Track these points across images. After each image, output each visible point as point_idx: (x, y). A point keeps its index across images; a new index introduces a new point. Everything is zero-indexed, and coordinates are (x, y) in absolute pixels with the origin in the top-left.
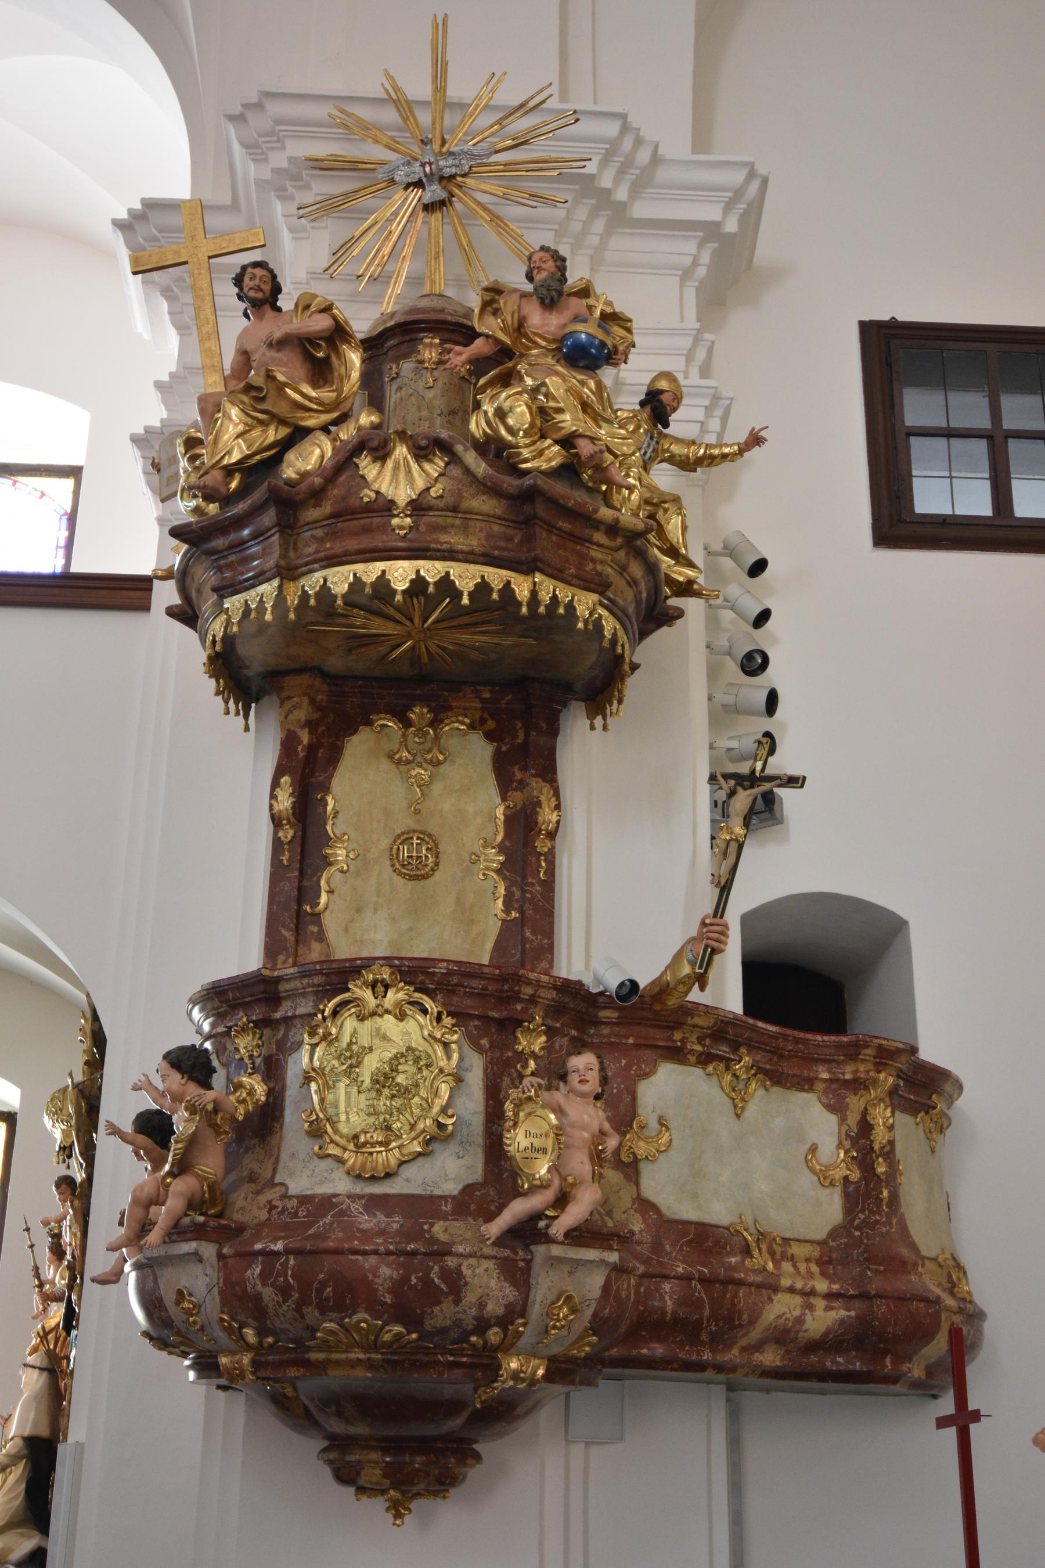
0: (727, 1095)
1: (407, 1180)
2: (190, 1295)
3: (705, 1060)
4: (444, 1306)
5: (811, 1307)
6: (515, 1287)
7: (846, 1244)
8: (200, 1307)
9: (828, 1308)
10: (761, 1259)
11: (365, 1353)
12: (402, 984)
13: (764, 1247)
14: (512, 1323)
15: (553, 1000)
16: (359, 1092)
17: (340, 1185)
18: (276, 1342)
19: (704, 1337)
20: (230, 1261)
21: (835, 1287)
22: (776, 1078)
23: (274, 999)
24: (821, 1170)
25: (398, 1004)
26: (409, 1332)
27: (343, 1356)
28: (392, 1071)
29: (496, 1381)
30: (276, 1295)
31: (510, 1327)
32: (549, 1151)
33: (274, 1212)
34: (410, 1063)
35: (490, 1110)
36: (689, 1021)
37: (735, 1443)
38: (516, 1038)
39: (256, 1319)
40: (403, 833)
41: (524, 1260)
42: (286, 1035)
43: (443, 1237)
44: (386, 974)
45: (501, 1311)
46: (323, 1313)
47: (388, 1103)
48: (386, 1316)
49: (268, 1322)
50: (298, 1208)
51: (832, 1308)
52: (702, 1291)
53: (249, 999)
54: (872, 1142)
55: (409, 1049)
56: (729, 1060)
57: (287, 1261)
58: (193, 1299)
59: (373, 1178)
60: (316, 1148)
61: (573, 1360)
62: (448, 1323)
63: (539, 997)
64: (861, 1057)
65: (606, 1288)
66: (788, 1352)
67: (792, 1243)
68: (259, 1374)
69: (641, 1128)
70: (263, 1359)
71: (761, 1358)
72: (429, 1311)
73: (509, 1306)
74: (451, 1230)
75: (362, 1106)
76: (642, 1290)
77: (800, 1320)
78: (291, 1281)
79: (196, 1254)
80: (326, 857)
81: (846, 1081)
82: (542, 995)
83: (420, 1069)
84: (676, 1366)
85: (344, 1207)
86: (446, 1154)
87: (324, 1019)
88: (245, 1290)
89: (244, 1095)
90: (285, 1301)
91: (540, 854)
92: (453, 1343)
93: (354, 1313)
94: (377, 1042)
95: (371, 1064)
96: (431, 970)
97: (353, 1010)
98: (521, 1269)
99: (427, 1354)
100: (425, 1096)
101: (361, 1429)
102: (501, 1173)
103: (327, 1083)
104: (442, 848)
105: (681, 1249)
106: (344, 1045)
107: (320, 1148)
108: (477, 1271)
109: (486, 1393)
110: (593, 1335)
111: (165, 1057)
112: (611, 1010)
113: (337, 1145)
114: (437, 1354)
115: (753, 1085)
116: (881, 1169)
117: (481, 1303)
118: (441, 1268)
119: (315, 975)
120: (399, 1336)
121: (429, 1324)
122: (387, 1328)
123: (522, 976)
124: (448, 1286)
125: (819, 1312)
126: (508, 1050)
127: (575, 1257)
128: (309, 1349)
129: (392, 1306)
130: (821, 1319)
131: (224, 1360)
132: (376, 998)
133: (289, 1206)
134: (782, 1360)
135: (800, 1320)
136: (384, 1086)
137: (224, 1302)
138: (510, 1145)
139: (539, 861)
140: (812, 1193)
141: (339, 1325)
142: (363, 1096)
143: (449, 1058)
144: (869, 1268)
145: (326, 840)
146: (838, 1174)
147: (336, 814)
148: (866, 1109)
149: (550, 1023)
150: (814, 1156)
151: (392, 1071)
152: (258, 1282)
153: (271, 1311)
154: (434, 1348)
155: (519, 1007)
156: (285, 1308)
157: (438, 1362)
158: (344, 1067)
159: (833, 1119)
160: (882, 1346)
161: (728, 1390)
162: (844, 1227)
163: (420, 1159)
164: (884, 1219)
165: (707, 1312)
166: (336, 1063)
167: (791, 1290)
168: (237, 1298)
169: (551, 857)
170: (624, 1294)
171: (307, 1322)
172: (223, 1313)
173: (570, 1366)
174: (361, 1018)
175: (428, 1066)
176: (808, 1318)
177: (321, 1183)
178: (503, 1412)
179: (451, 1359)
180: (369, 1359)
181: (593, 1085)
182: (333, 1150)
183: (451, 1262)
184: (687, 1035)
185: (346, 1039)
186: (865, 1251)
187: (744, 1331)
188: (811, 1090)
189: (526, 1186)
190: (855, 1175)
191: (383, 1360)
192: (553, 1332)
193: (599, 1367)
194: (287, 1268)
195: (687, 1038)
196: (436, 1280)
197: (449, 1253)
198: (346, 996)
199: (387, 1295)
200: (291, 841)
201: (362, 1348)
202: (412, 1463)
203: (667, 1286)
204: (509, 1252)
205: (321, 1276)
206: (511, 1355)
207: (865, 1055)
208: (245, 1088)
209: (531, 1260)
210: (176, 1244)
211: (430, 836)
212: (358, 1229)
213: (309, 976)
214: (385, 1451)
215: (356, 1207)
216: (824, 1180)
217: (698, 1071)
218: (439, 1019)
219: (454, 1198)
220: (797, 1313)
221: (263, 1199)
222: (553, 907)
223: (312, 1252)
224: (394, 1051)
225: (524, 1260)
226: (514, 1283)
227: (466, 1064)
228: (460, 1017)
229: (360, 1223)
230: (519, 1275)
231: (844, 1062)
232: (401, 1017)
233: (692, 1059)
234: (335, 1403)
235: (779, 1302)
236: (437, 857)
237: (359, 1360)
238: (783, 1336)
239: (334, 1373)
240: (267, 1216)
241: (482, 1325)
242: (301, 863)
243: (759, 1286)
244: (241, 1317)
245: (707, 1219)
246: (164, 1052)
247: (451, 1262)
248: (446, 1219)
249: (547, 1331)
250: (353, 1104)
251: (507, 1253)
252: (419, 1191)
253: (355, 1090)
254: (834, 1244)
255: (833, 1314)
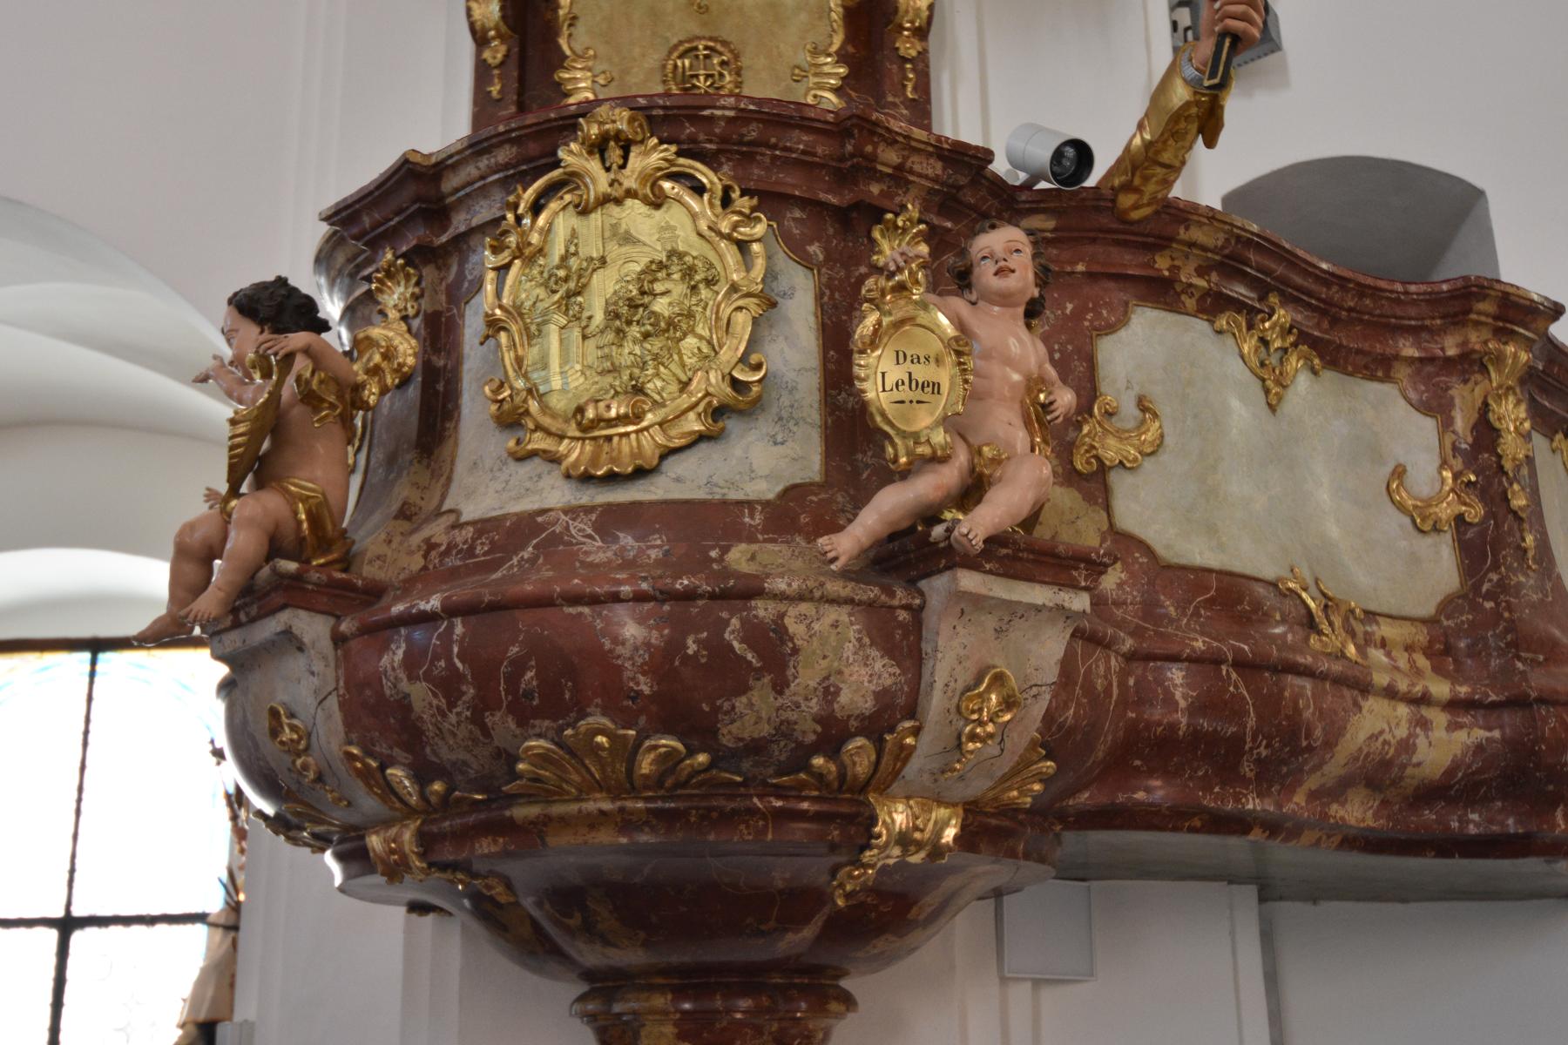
0: (1251, 370)
1: (678, 480)
2: (292, 715)
3: (1212, 305)
4: (755, 696)
5: (1424, 724)
6: (892, 658)
7: (1472, 623)
8: (309, 735)
9: (1453, 727)
10: (1332, 638)
11: (613, 800)
12: (655, 141)
13: (1337, 621)
14: (892, 730)
15: (935, 180)
16: (584, 337)
17: (554, 494)
18: (450, 790)
19: (1247, 769)
20: (354, 644)
21: (1463, 690)
22: (1331, 356)
23: (438, 213)
24: (1416, 507)
25: (652, 179)
26: (691, 752)
27: (573, 808)
28: (643, 293)
29: (869, 847)
30: (435, 695)
31: (888, 737)
32: (945, 389)
33: (433, 553)
34: (676, 276)
35: (832, 367)
36: (1183, 234)
37: (1272, 980)
38: (873, 241)
39: (406, 747)
40: (681, 43)
41: (907, 607)
42: (461, 274)
43: (746, 568)
44: (621, 120)
45: (867, 705)
46: (522, 723)
47: (637, 351)
48: (642, 720)
49: (428, 750)
50: (474, 540)
51: (1460, 726)
52: (1241, 684)
53: (397, 219)
54: (1500, 457)
55: (672, 253)
56: (1251, 312)
57: (451, 628)
58: (295, 722)
59: (612, 478)
60: (512, 443)
61: (1010, 811)
62: (765, 730)
63: (911, 172)
64: (1473, 316)
65: (1067, 666)
66: (1385, 803)
67: (1380, 619)
68: (435, 858)
69: (1110, 414)
70: (435, 829)
71: (1341, 813)
72: (726, 706)
73: (882, 696)
74: (763, 557)
75: (590, 360)
76: (1131, 682)
77: (1407, 746)
78: (459, 665)
79: (288, 633)
80: (559, 84)
81: (1448, 360)
82: (917, 168)
83: (694, 288)
84: (1197, 823)
85: (558, 529)
86: (752, 436)
87: (519, 219)
88: (380, 694)
89: (377, 358)
90: (451, 705)
91: (905, 60)
92: (779, 774)
93: (583, 715)
94: (614, 251)
95: (603, 289)
96: (707, 113)
97: (568, 198)
98: (902, 625)
99: (731, 797)
100: (706, 333)
101: (630, 956)
102: (853, 434)
103: (527, 329)
104: (745, 61)
105: (1196, 614)
106: (556, 260)
107: (518, 442)
108: (816, 626)
109: (851, 877)
110: (1047, 757)
111: (230, 302)
112: (1042, 217)
113: (548, 433)
114: (751, 796)
115: (1294, 362)
116: (1519, 502)
117: (826, 689)
118: (743, 622)
119: (500, 145)
120: (669, 761)
121: (730, 733)
122: (647, 743)
123: (876, 124)
124: (760, 657)
125: (1439, 733)
126: (858, 264)
127: (1005, 596)
128: (512, 799)
129: (653, 698)
130: (1443, 746)
131: (375, 842)
132: (608, 170)
133: (459, 539)
134: (1376, 816)
135: (1407, 746)
136: (629, 323)
137: (350, 723)
138: (863, 380)
139: (903, 70)
140: (1403, 544)
141: (556, 744)
142: (591, 343)
143: (748, 264)
144: (1519, 658)
145: (558, 60)
146: (1446, 510)
147: (573, 20)
148: (1486, 404)
149: (936, 221)
150: (1401, 484)
151: (643, 293)
152: (402, 675)
153: (430, 729)
154: (744, 784)
155: (875, 189)
156: (453, 718)
157: (753, 812)
158: (557, 297)
159: (1429, 425)
160: (1551, 787)
161: (1262, 899)
162: (1464, 597)
163: (703, 446)
164: (1532, 582)
165: (1251, 721)
166: (541, 292)
167: (1391, 693)
168: (374, 714)
169: (922, 64)
170: (1100, 684)
171: (496, 743)
172: (350, 743)
173: (1006, 823)
174: (584, 211)
175: (710, 282)
176: (1421, 742)
177: (518, 498)
178: (892, 913)
179: (779, 804)
180: (622, 810)
181: (1023, 279)
182: (539, 442)
183: (763, 610)
184: (1177, 263)
185: (557, 250)
186: (1507, 631)
187: (1315, 761)
188: (1387, 378)
189: (903, 460)
190: (1475, 512)
191: (648, 810)
192: (971, 746)
193: (1058, 828)
194: (452, 642)
195: (1179, 268)
196: (736, 644)
197: (759, 593)
198: (556, 173)
199: (642, 678)
200: (502, 64)
201: (609, 791)
202: (729, 1011)
203: (1176, 675)
204: (876, 590)
205: (514, 650)
206: (894, 798)
207: (1479, 313)
208: (378, 346)
209: (922, 607)
210: (258, 624)
211: (725, 43)
212: (582, 562)
213: (487, 151)
214: (680, 992)
215: (580, 528)
216: (1422, 522)
217: (1201, 325)
218: (726, 201)
219: (766, 504)
220: (1402, 732)
221: (416, 539)
222: (927, 66)
223: (494, 607)
224: (645, 261)
225: (907, 607)
226: (890, 651)
227: (782, 284)
228: (770, 201)
229: (587, 553)
230: (904, 642)
231: (1442, 331)
232: (657, 201)
233: (1190, 303)
234: (567, 898)
235: (1371, 711)
236: (738, 74)
237: (602, 812)
238: (1378, 774)
239: (559, 840)
240: (422, 562)
241: (833, 735)
242: (520, 94)
243: (1339, 681)
244: (382, 748)
245: (1237, 566)
246: (230, 294)
247: (763, 610)
248: (751, 540)
249: (959, 746)
250: (573, 356)
251: (873, 592)
252: (701, 495)
253: (576, 333)
254: (1450, 623)
255: (1461, 736)
